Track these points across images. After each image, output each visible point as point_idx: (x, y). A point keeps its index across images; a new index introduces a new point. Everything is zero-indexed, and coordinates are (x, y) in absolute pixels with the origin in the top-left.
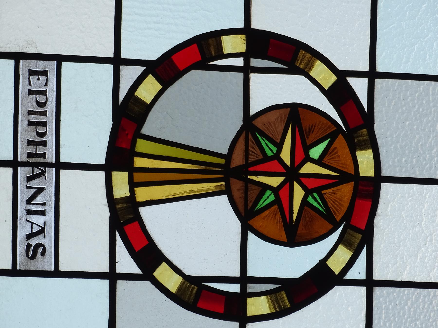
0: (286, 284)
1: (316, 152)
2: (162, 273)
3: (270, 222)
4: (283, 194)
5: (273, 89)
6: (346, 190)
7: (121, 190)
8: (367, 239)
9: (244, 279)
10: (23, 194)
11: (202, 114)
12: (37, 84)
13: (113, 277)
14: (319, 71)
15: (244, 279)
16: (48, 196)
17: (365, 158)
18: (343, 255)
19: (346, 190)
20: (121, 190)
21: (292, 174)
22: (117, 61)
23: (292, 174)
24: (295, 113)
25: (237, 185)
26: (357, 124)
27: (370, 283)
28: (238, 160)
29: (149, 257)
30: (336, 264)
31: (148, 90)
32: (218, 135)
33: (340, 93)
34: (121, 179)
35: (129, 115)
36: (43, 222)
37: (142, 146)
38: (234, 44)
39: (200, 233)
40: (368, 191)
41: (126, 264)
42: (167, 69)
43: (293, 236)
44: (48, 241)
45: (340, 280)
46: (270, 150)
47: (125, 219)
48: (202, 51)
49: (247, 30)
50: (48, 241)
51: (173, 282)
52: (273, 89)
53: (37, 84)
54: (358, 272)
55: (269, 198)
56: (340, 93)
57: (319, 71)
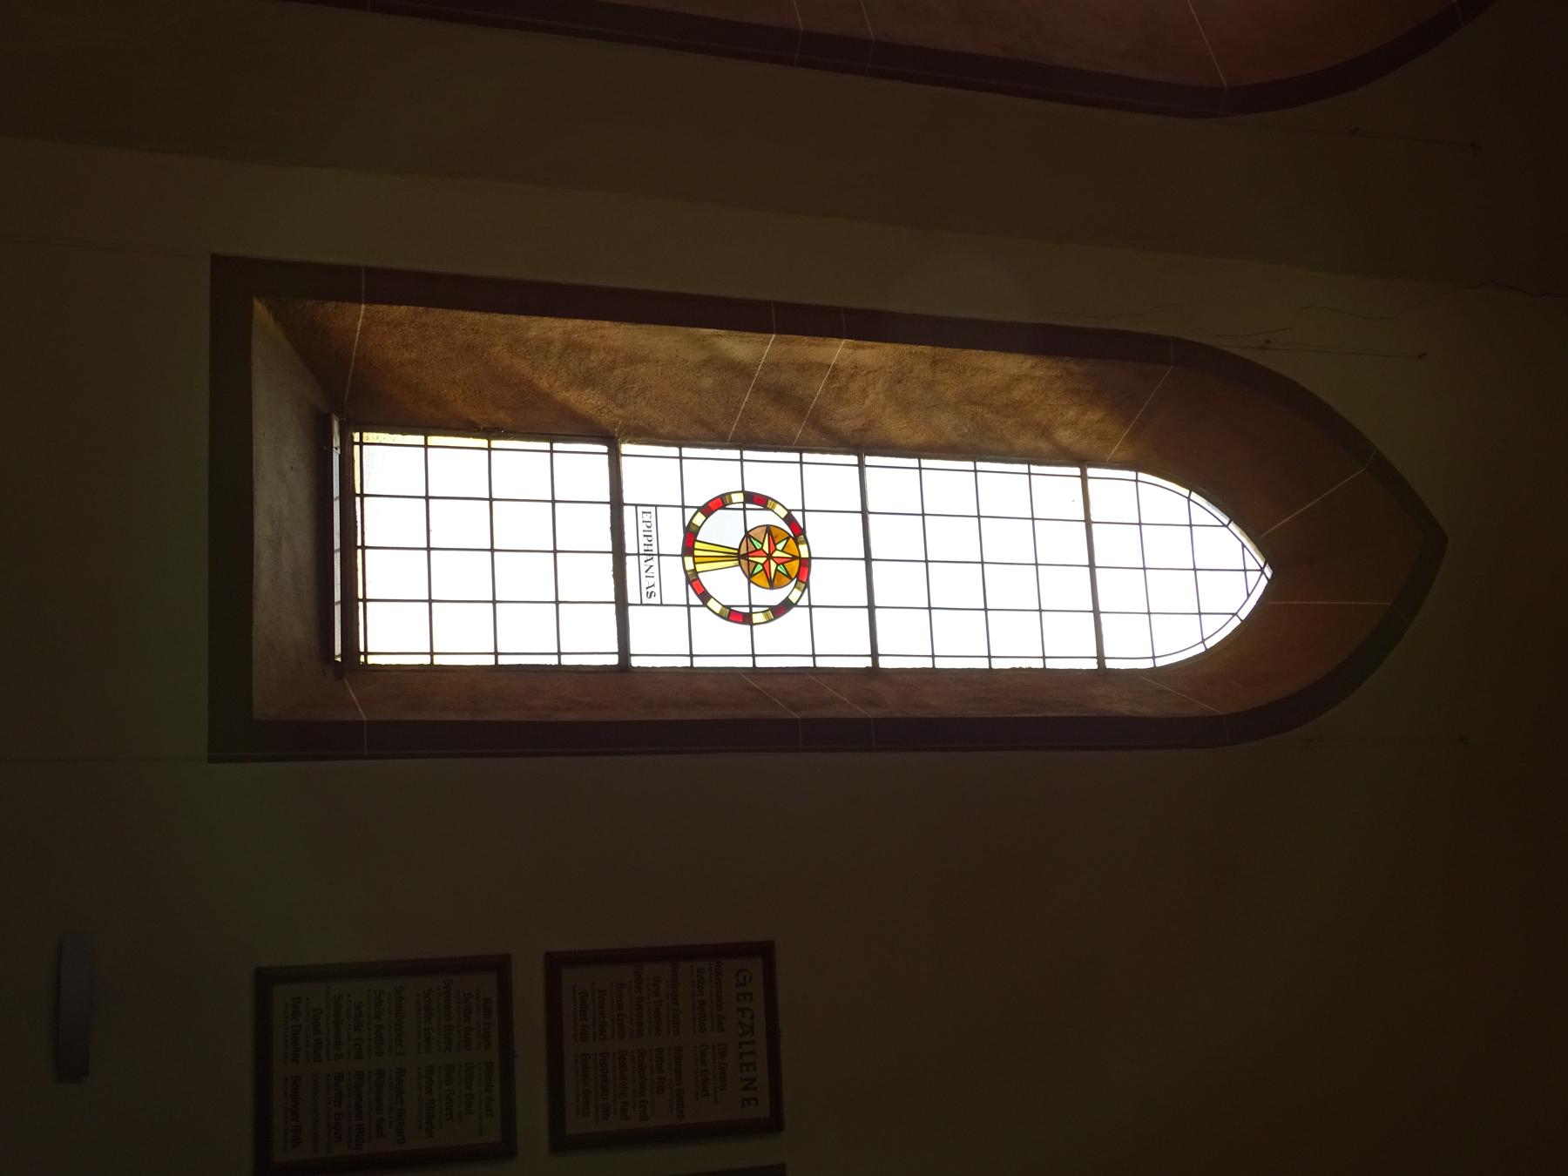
0: (723, 507)
1: (780, 546)
2: (711, 603)
3: (761, 579)
4: (766, 570)
5: (758, 518)
6: (796, 563)
7: (690, 566)
8: (807, 585)
9: (744, 509)
10: (644, 569)
11: (724, 530)
12: (647, 517)
13: (689, 606)
14: (778, 509)
15: (751, 606)
16: (655, 569)
17: (803, 548)
18: (797, 593)
19: (796, 563)
20: (690, 566)
21: (769, 556)
22: (683, 507)
23: (769, 556)
24: (769, 529)
25: (744, 562)
26: (798, 533)
27: (810, 607)
28: (743, 551)
29: (705, 597)
30: (793, 599)
31: (699, 519)
32: (734, 539)
33: (789, 519)
34: (689, 560)
35: (691, 534)
36: (810, 534)
37: (697, 545)
38: (757, 618)
39: (728, 584)
40: (805, 564)
41: (694, 600)
42: (707, 510)
43: (772, 584)
44: (656, 589)
45: (700, 509)
46: (758, 546)
47: (692, 580)
48: (721, 502)
49: (752, 625)
50: (656, 589)
51: (718, 608)
52: (758, 518)
53: (647, 517)
54: (804, 601)
55: (759, 568)
56: (789, 519)
57: (778, 509)
